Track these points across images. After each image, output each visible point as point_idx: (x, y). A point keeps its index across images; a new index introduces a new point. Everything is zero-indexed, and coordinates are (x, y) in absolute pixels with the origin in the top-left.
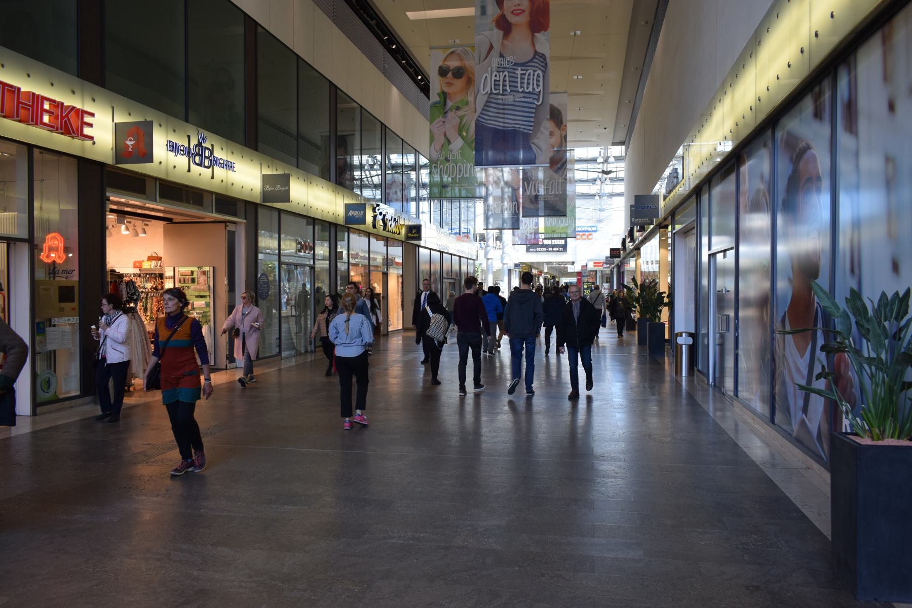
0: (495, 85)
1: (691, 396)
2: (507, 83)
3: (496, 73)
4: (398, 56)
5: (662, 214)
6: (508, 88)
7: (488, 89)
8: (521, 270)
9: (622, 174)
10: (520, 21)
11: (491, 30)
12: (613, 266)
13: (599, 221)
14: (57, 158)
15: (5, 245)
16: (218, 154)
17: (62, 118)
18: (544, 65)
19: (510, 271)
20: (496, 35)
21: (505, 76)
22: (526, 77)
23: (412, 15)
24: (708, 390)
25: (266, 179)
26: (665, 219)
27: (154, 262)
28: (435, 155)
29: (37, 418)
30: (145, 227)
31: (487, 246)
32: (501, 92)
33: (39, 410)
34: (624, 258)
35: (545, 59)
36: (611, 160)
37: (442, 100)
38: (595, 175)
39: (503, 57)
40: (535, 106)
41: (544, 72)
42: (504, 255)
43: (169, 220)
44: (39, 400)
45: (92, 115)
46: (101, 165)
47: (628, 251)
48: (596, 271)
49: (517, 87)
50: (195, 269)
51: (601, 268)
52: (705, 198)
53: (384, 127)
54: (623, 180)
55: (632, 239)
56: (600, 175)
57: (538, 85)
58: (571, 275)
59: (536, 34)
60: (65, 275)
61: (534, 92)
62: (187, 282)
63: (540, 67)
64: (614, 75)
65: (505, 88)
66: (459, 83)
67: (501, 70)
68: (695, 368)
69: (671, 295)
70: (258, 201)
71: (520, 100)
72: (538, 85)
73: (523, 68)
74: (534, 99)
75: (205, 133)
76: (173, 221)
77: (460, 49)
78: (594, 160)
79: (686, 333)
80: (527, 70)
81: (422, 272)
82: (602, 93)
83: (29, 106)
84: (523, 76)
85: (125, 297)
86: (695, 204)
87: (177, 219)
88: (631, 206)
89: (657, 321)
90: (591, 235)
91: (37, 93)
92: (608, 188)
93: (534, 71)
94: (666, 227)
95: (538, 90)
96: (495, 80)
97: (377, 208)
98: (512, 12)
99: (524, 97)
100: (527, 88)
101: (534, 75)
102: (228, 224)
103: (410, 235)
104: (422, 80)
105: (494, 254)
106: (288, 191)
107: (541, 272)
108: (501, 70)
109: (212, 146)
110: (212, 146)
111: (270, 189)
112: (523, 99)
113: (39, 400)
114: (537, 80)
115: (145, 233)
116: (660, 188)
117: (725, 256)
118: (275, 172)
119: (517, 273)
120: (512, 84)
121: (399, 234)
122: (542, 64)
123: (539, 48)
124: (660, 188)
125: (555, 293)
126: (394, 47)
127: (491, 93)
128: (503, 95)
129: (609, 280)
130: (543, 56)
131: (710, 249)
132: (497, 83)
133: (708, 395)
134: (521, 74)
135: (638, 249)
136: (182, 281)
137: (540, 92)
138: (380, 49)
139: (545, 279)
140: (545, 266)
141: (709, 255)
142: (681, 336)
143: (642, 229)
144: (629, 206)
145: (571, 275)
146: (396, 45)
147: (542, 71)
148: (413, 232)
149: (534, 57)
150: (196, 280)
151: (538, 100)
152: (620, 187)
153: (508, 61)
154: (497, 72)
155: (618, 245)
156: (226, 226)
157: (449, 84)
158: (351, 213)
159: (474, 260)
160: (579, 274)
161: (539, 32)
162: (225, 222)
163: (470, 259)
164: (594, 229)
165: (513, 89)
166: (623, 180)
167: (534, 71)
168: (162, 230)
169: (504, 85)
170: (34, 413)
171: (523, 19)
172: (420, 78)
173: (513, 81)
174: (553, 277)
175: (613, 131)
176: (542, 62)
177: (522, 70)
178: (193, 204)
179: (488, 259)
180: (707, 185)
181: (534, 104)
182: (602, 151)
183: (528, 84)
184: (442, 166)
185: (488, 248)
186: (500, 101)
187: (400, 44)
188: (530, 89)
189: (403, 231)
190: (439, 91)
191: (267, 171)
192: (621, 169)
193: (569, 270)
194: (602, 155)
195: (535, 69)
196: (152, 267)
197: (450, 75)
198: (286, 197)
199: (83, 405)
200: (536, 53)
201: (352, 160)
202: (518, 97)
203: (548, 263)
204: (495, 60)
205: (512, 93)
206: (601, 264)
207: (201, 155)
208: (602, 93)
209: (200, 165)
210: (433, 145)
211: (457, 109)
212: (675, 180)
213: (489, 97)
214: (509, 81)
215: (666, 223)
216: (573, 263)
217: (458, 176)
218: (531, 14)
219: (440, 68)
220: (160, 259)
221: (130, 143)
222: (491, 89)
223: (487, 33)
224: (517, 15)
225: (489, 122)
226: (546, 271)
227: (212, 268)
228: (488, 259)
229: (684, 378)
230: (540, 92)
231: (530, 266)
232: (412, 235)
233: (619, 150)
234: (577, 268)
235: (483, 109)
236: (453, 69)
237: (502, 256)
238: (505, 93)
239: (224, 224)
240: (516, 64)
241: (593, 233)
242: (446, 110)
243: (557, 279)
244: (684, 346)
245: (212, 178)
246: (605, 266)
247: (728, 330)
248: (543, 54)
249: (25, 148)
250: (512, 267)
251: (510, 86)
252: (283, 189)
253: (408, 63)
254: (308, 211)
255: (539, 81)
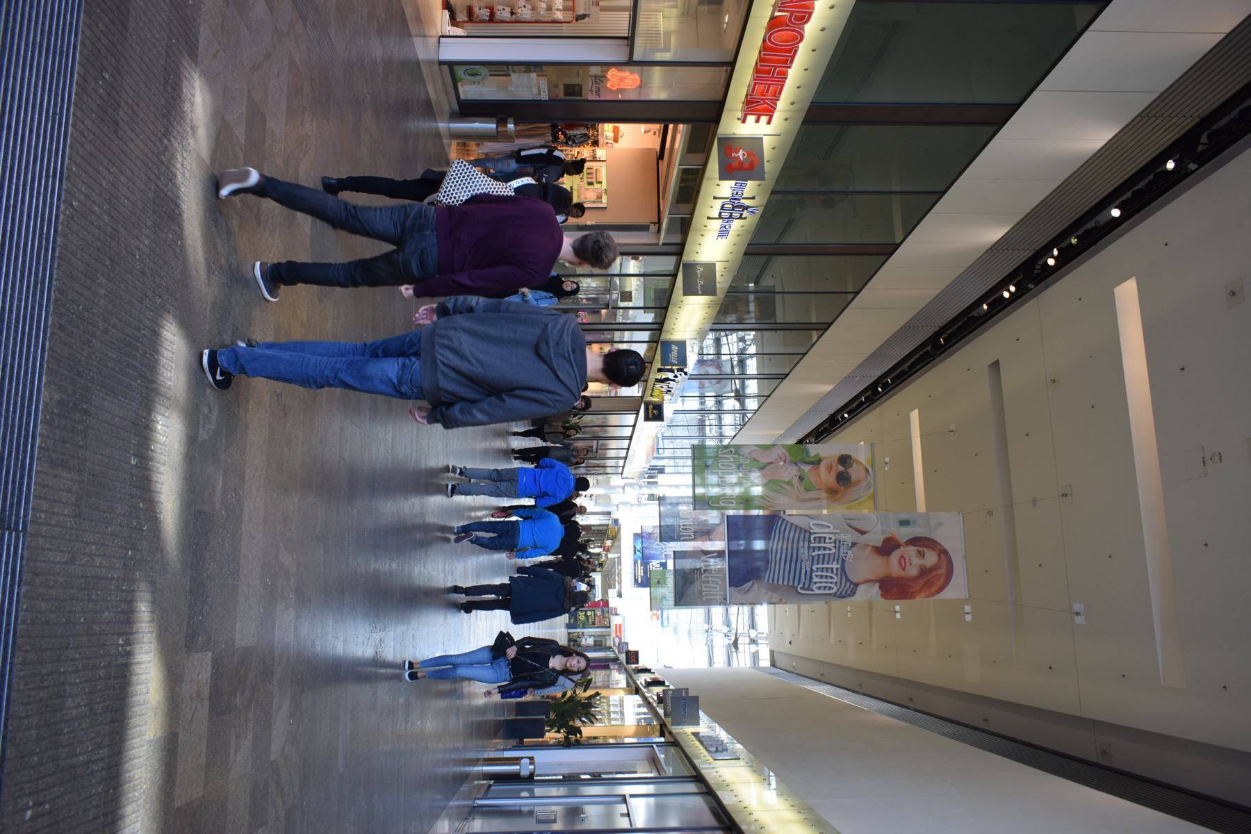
0: (820, 537)
1: (464, 778)
2: (822, 552)
3: (834, 538)
4: (870, 393)
5: (676, 729)
6: (817, 553)
7: (815, 530)
8: (610, 527)
9: (735, 664)
10: (892, 566)
11: (883, 532)
12: (616, 651)
13: (676, 630)
14: (722, 82)
15: (626, 35)
16: (736, 224)
17: (763, 100)
18: (843, 594)
19: (609, 513)
20: (877, 538)
21: (830, 549)
22: (829, 574)
23: (915, 415)
24: (469, 799)
25: (710, 267)
26: (670, 733)
27: (612, 135)
28: (745, 451)
29: (436, 67)
30: (652, 132)
31: (640, 487)
32: (812, 545)
33: (446, 68)
34: (626, 670)
35: (849, 596)
36: (754, 648)
37: (812, 460)
38: (734, 625)
39: (851, 547)
40: (796, 584)
41: (835, 595)
42: (629, 506)
43: (661, 156)
44: (456, 67)
45: (769, 122)
46: (717, 120)
47: (635, 676)
48: (609, 627)
49: (818, 564)
50: (604, 186)
51: (613, 635)
52: (691, 787)
53: (783, 377)
54: (729, 665)
55: (649, 684)
56: (734, 631)
57: (819, 588)
58: (605, 592)
59: (878, 584)
60: (594, 89)
61: (812, 584)
62: (589, 176)
63: (841, 589)
64: (851, 657)
65: (816, 549)
66: (828, 478)
67: (837, 545)
68: (492, 782)
69: (578, 744)
70: (685, 258)
71: (803, 567)
72: (819, 588)
73: (839, 570)
74: (804, 583)
75: (759, 212)
76: (660, 161)
77: (872, 480)
78: (753, 626)
79: (534, 769)
80: (837, 575)
81: (605, 418)
82: (832, 640)
83: (773, 74)
84: (830, 570)
85: (570, 132)
86: (687, 775)
87: (663, 165)
88: (687, 690)
89: (547, 728)
90: (658, 619)
91: (787, 81)
92: (721, 643)
93: (836, 583)
94: (662, 735)
95: (814, 588)
96: (825, 538)
97: (682, 373)
98: (902, 557)
99: (806, 571)
100: (816, 576)
101: (831, 583)
102: (657, 225)
103: (651, 406)
104: (843, 417)
105: (631, 495)
106: (696, 294)
107: (607, 550)
108: (837, 545)
109: (745, 218)
110: (745, 218)
111: (698, 272)
112: (803, 571)
113: (456, 67)
114: (825, 587)
115: (645, 132)
116: (705, 725)
117: (623, 815)
118: (718, 278)
119: (606, 522)
120: (821, 557)
121: (652, 396)
122: (844, 592)
123: (861, 588)
124: (705, 725)
125: (581, 570)
126: (880, 389)
127: (810, 533)
128: (809, 547)
129: (599, 646)
130: (853, 593)
131: (632, 796)
132: (822, 540)
133: (465, 799)
134: (832, 569)
135: (637, 691)
136: (590, 171)
137: (812, 590)
138: (877, 373)
139: (599, 554)
140: (616, 555)
141: (624, 796)
142: (531, 764)
143: (660, 700)
144: (686, 687)
145: (605, 592)
146: (892, 384)
147: (836, 593)
148: (655, 411)
149: (851, 583)
150: (591, 187)
151: (803, 588)
152: (720, 662)
153: (847, 553)
154: (835, 541)
155: (643, 663)
156: (654, 223)
157: (830, 468)
158: (674, 348)
159: (622, 474)
160: (606, 603)
161: (881, 588)
162: (659, 222)
163: (625, 462)
164: (665, 622)
165: (816, 559)
166: (729, 665)
167: (836, 583)
168: (649, 146)
169: (819, 548)
170: (441, 63)
171: (895, 570)
172: (846, 415)
173: (823, 558)
174: (601, 565)
175: (787, 652)
176: (846, 592)
177: (837, 569)
178: (680, 187)
179: (623, 488)
180: (705, 790)
181: (799, 584)
182: (765, 635)
183: (822, 577)
184: (732, 460)
185: (637, 488)
186: (801, 544)
187: (882, 396)
188: (815, 579)
189: (655, 399)
190: (822, 455)
191: (719, 268)
192: (742, 661)
193: (610, 591)
194: (759, 635)
195: (839, 584)
196: (606, 133)
197: (841, 468)
198: (689, 291)
199: (449, 103)
200: (857, 585)
201: (711, 447)
202: (806, 565)
203: (619, 558)
204: (848, 537)
205: (811, 558)
206: (619, 634)
207: (733, 210)
208: (832, 640)
209: (722, 208)
210: (757, 448)
211: (800, 477)
212: (713, 749)
213: (806, 531)
214: (824, 555)
215: (667, 734)
216: (620, 595)
217: (720, 471)
218: (900, 578)
219: (849, 457)
220: (616, 140)
221: (740, 153)
222: (815, 533)
223: (879, 528)
224: (900, 562)
225: (778, 532)
226: (610, 556)
227: (605, 206)
228: (623, 488)
229: (480, 768)
230: (812, 590)
231: (615, 537)
232: (650, 410)
233: (765, 662)
234: (613, 602)
235: (792, 524)
236: (847, 473)
237: (629, 503)
238: (811, 550)
239: (657, 221)
240: (843, 561)
241: (660, 621)
242: (799, 465)
243: (598, 569)
244: (518, 767)
245: (709, 218)
246: (617, 640)
247: (539, 822)
248: (854, 593)
249: (729, 59)
250: (614, 516)
251: (819, 555)
252: (699, 288)
253: (862, 403)
254: (675, 304)
255: (824, 590)
